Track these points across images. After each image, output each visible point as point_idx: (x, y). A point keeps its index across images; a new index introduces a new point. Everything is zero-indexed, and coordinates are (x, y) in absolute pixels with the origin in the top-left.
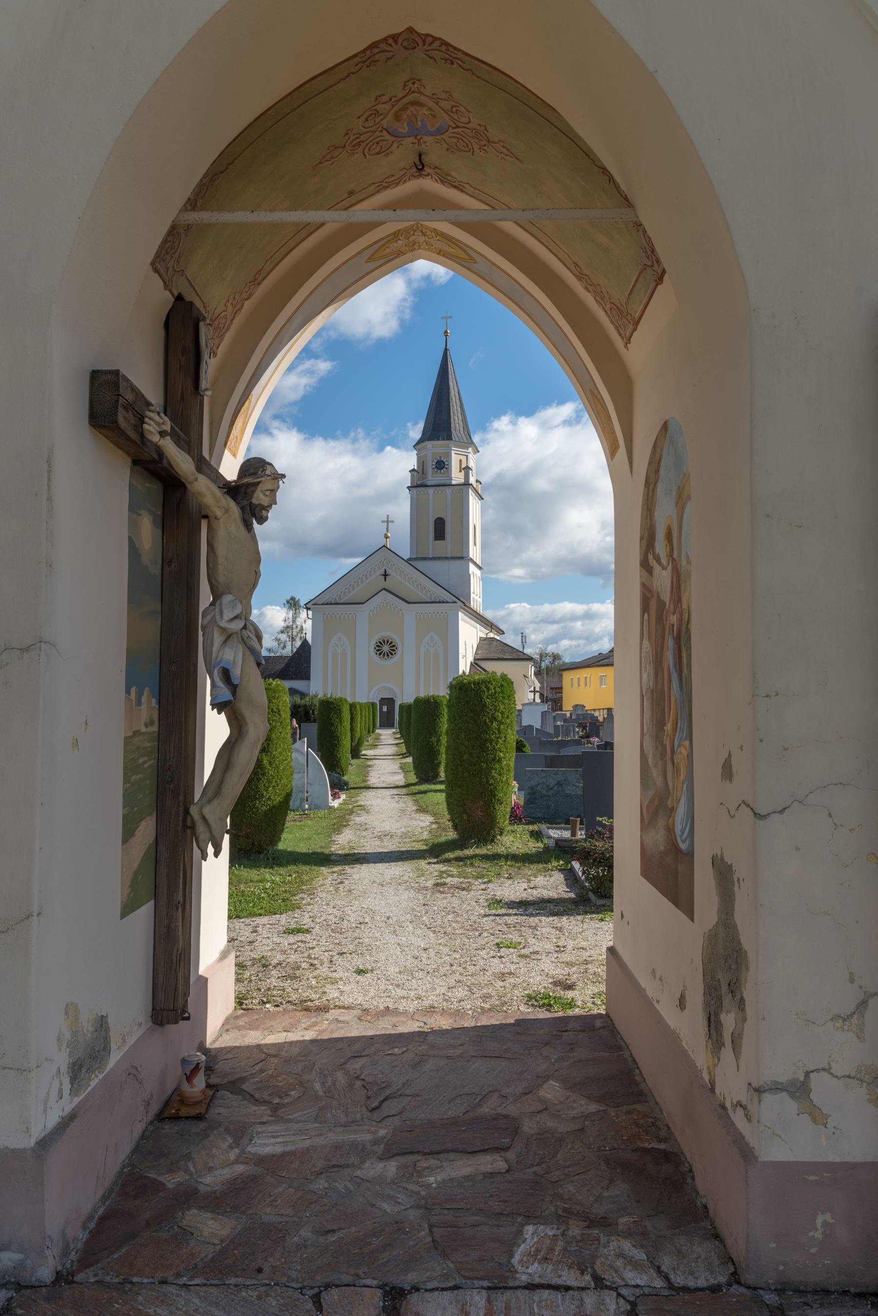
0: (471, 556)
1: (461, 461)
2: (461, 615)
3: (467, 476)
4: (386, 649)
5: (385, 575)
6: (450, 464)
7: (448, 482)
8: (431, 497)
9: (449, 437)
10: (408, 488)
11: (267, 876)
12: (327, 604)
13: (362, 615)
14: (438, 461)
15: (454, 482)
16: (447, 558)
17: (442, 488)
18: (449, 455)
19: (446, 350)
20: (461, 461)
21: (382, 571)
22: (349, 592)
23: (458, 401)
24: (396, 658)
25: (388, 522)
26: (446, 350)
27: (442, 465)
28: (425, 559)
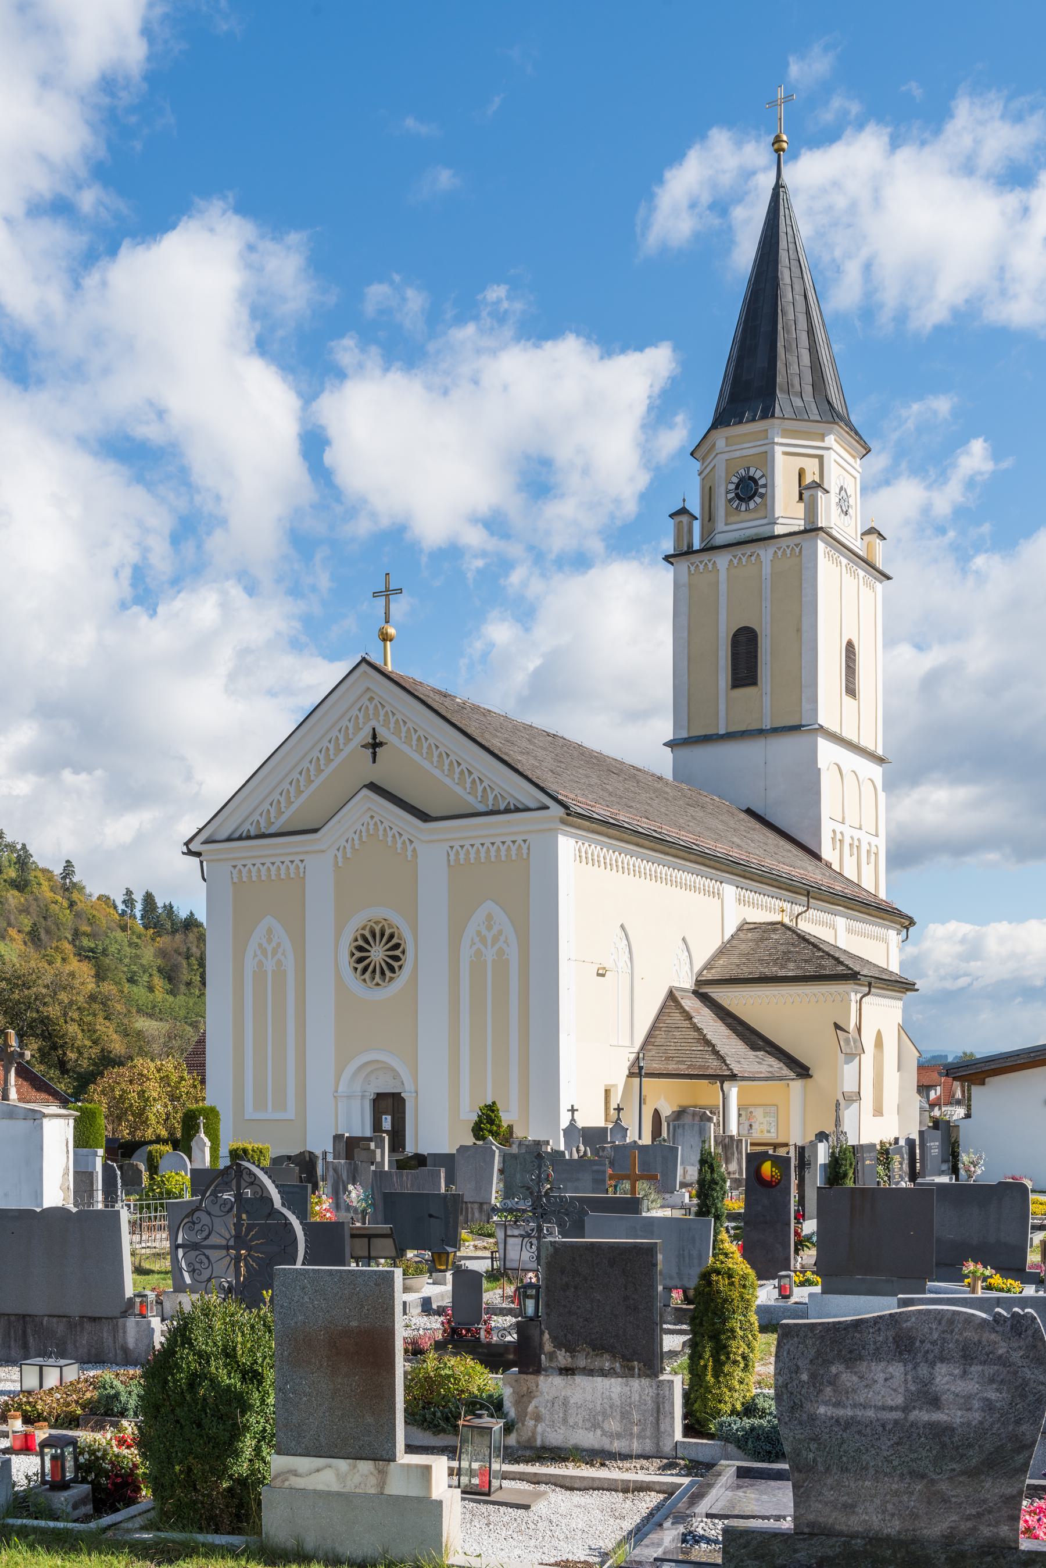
0: (824, 718)
1: (801, 473)
2: (568, 847)
3: (811, 511)
4: (378, 954)
5: (375, 744)
6: (770, 485)
7: (765, 531)
8: (723, 576)
9: (773, 416)
10: (667, 558)
11: (828, 1550)
12: (240, 838)
13: (318, 862)
14: (742, 480)
15: (779, 530)
16: (761, 732)
17: (749, 549)
18: (766, 459)
20: (801, 473)
21: (364, 735)
22: (290, 803)
24: (403, 977)
27: (750, 489)
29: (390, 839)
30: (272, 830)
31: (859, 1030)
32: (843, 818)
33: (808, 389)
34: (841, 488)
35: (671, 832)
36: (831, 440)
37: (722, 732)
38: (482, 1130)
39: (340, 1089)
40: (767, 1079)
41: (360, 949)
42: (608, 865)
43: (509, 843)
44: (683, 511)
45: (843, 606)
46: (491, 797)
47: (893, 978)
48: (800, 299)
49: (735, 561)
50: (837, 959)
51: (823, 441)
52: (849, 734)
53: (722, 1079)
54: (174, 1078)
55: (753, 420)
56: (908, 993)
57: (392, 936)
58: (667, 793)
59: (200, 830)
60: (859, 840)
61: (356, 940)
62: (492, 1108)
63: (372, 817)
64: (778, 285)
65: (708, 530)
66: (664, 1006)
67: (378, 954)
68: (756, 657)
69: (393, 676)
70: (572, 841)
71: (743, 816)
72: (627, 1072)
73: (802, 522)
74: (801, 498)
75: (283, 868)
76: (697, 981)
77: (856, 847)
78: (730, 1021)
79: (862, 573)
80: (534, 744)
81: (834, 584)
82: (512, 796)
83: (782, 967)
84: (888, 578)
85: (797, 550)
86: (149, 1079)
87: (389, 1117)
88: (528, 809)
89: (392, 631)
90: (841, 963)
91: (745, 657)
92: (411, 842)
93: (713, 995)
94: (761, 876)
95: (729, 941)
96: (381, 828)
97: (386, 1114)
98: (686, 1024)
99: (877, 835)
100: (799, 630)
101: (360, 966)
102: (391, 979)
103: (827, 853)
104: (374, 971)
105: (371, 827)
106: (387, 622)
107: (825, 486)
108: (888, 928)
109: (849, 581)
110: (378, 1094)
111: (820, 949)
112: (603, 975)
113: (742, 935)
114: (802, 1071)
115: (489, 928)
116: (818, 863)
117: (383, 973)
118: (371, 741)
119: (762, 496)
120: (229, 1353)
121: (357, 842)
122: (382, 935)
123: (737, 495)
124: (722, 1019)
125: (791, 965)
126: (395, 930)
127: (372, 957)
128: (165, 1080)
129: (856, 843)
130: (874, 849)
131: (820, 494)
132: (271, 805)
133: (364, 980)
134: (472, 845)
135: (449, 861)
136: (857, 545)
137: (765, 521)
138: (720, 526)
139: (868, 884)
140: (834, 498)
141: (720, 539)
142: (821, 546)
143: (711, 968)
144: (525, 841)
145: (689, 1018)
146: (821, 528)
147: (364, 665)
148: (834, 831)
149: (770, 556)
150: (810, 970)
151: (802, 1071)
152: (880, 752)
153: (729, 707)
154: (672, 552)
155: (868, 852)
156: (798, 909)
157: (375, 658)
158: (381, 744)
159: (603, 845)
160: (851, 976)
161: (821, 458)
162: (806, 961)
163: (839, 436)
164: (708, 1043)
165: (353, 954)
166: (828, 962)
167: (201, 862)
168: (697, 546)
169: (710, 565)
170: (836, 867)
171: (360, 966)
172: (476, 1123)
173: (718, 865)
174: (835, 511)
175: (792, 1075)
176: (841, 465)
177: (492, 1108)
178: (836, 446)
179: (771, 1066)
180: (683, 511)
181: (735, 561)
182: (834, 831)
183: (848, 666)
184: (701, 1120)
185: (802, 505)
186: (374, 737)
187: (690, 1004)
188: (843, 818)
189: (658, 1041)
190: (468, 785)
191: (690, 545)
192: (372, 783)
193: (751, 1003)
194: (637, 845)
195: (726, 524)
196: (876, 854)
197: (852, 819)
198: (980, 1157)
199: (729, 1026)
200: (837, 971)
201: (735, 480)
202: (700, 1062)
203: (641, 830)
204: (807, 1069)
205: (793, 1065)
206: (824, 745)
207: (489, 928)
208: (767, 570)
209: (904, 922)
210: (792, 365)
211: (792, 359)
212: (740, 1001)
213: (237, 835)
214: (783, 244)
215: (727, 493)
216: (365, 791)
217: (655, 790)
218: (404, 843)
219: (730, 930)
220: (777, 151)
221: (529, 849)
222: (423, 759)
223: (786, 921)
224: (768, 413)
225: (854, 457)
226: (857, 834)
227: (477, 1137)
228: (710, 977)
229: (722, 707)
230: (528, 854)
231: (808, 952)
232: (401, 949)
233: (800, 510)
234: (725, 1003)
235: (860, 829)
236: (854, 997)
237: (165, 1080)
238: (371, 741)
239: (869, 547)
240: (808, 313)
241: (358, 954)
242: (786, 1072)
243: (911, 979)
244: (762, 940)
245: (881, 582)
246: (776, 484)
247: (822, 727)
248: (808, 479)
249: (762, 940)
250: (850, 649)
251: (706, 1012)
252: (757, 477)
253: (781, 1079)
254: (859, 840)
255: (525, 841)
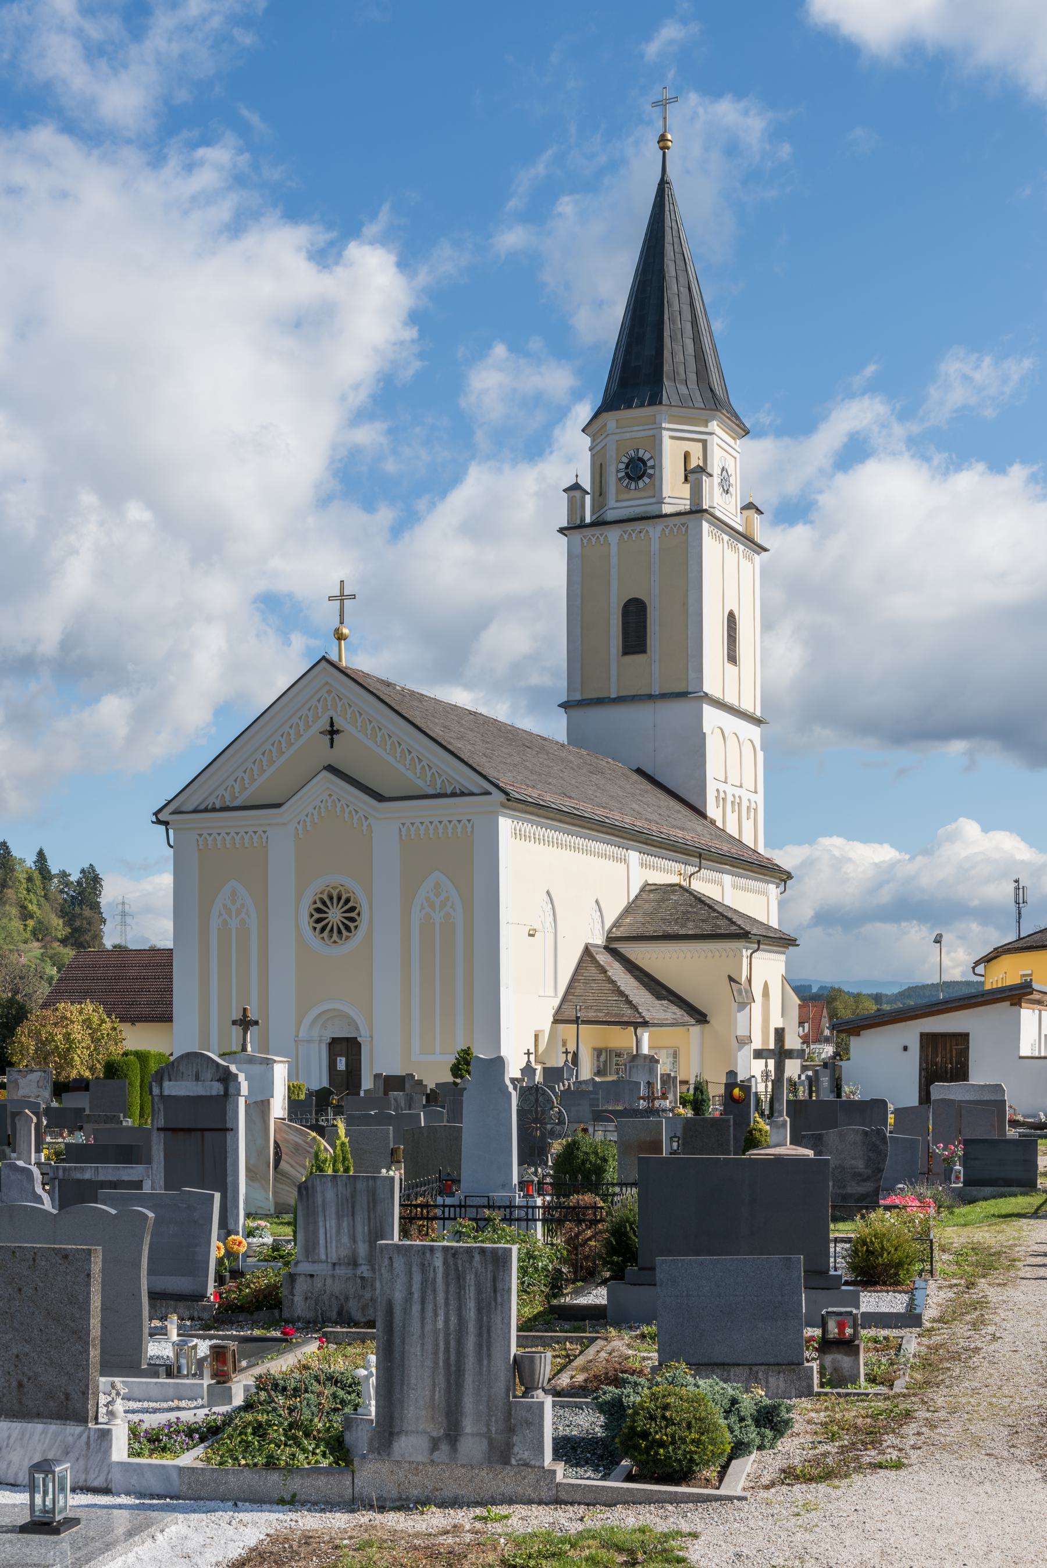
0: (711, 686)
1: (687, 456)
2: (506, 825)
3: (697, 493)
4: (336, 916)
5: (333, 732)
6: (658, 466)
7: (652, 510)
8: (614, 550)
9: (661, 403)
10: (562, 530)
13: (281, 837)
14: (631, 460)
15: (667, 509)
16: (650, 697)
18: (656, 443)
19: (663, 185)
20: (687, 456)
21: (323, 724)
22: (253, 780)
23: (686, 309)
24: (358, 937)
25: (342, 597)
26: (663, 185)
27: (639, 469)
28: (599, 702)
29: (346, 815)
30: (236, 804)
31: (750, 981)
32: (726, 778)
33: (692, 377)
34: (723, 469)
35: (587, 809)
36: (714, 426)
37: (613, 696)
38: (460, 1070)
39: (300, 1035)
40: (672, 1025)
41: (318, 910)
42: (538, 840)
43: (455, 822)
44: (576, 487)
45: (727, 579)
46: (439, 782)
47: (778, 936)
48: (684, 291)
49: (626, 537)
50: (730, 920)
51: (707, 426)
52: (731, 699)
53: (636, 1025)
54: (96, 1020)
55: (642, 405)
56: (791, 948)
57: (348, 901)
58: (571, 762)
59: (169, 802)
60: (740, 797)
61: (315, 903)
62: (467, 1052)
63: (330, 795)
64: (664, 277)
65: (599, 503)
66: (581, 961)
67: (335, 915)
68: (645, 627)
69: (349, 672)
70: (510, 821)
71: (635, 777)
72: (552, 1019)
73: (688, 502)
74: (686, 479)
75: (247, 837)
76: (608, 937)
77: (737, 804)
78: (637, 973)
79: (741, 547)
80: (462, 725)
81: (716, 554)
82: (458, 782)
83: (683, 926)
84: (766, 550)
85: (684, 529)
86: (73, 1022)
87: (344, 1059)
88: (472, 794)
89: (345, 631)
90: (734, 923)
91: (635, 627)
92: (366, 818)
93: (622, 950)
94: (661, 842)
95: (634, 901)
96: (339, 805)
97: (341, 1056)
98: (602, 976)
99: (756, 792)
100: (685, 604)
101: (319, 926)
102: (347, 938)
103: (713, 811)
104: (332, 930)
105: (329, 804)
106: (342, 623)
107: (709, 470)
108: (768, 882)
109: (731, 556)
110: (333, 1039)
111: (715, 910)
112: (533, 935)
113: (644, 896)
114: (700, 1017)
115: (437, 895)
116: (704, 822)
117: (340, 932)
118: (329, 728)
119: (650, 476)
120: (596, 1153)
121: (316, 817)
122: (339, 899)
123: (627, 474)
124: (630, 971)
125: (691, 925)
126: (351, 894)
127: (330, 918)
128: (87, 1022)
129: (737, 800)
130: (753, 805)
131: (704, 478)
132: (235, 781)
133: (323, 938)
134: (422, 823)
135: (401, 836)
136: (736, 521)
137: (653, 500)
138: (612, 502)
139: (748, 840)
140: (716, 479)
141: (610, 516)
142: (705, 526)
143: (620, 926)
144: (469, 821)
145: (604, 971)
146: (706, 510)
147: (323, 663)
148: (718, 790)
149: (658, 534)
150: (707, 929)
151: (700, 1017)
152: (758, 713)
153: (622, 673)
154: (565, 525)
155: (748, 808)
156: (691, 869)
157: (333, 657)
158: (337, 732)
159: (533, 822)
160: (743, 935)
161: (704, 443)
162: (703, 921)
163: (722, 422)
164: (621, 993)
165: (312, 916)
166: (721, 922)
167: (167, 830)
168: (588, 520)
169: (602, 539)
170: (719, 824)
171: (319, 926)
172: (454, 1065)
173: (625, 835)
174: (717, 491)
175: (693, 1021)
176: (724, 450)
177: (467, 1052)
178: (718, 431)
179: (674, 1013)
180: (576, 487)
181: (626, 537)
182: (718, 790)
183: (729, 635)
184: (651, 1061)
185: (688, 486)
186: (332, 724)
187: (604, 958)
188: (726, 778)
189: (578, 992)
190: (418, 771)
191: (583, 519)
192: (329, 765)
193: (656, 958)
194: (560, 821)
195: (617, 501)
196: (755, 810)
197: (734, 779)
198: (857, 1089)
199: (636, 978)
200: (731, 930)
201: (626, 460)
202: (615, 1010)
203: (565, 809)
204: (704, 1016)
205: (692, 1012)
206: (708, 710)
207: (437, 895)
208: (655, 546)
209: (781, 876)
210: (677, 354)
211: (678, 348)
212: (644, 955)
213: (202, 807)
214: (668, 238)
215: (618, 471)
216: (325, 773)
217: (563, 760)
218: (359, 819)
219: (635, 891)
220: (662, 148)
221: (472, 827)
222: (369, 745)
223: (683, 883)
224: (655, 399)
225: (734, 439)
226: (738, 792)
227: (455, 1076)
228: (619, 934)
229: (614, 672)
230: (472, 831)
231: (704, 912)
232: (356, 912)
233: (685, 491)
234: (632, 958)
235: (741, 787)
236: (746, 953)
237: (87, 1022)
238: (329, 728)
239: (748, 522)
240: (692, 304)
241: (317, 916)
242: (687, 1018)
243: (793, 935)
244: (663, 900)
245: (758, 554)
246: (664, 465)
247: (706, 694)
248: (694, 463)
249: (663, 900)
250: (731, 617)
251: (617, 965)
252: (646, 458)
253: (683, 1024)
254: (740, 797)
255: (469, 821)
